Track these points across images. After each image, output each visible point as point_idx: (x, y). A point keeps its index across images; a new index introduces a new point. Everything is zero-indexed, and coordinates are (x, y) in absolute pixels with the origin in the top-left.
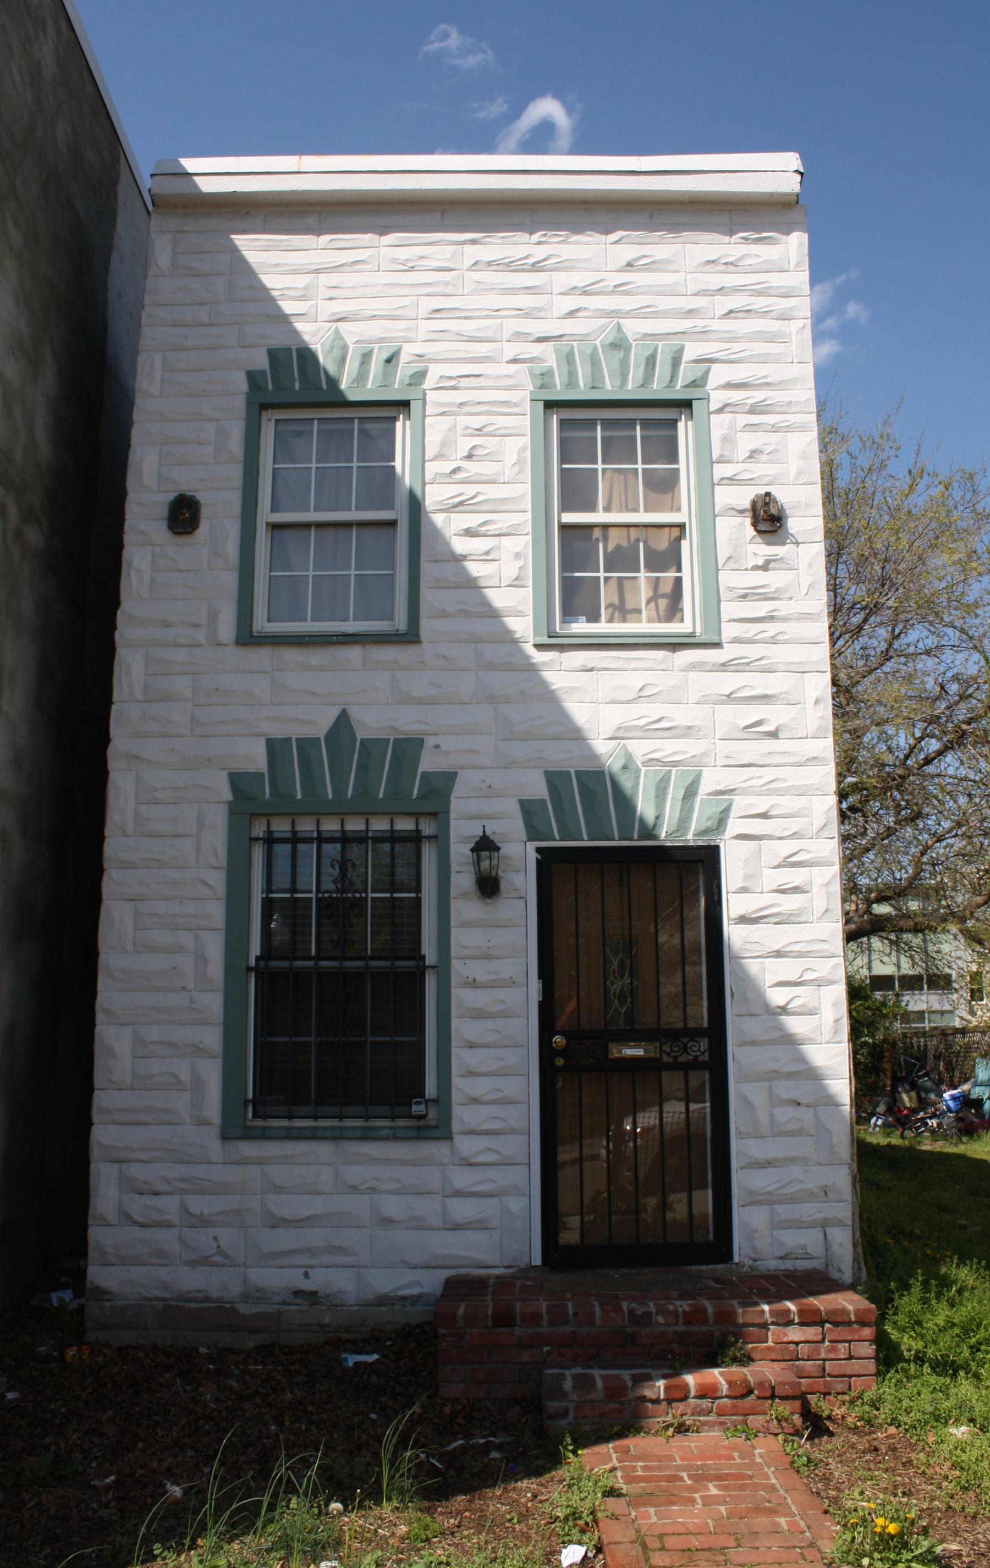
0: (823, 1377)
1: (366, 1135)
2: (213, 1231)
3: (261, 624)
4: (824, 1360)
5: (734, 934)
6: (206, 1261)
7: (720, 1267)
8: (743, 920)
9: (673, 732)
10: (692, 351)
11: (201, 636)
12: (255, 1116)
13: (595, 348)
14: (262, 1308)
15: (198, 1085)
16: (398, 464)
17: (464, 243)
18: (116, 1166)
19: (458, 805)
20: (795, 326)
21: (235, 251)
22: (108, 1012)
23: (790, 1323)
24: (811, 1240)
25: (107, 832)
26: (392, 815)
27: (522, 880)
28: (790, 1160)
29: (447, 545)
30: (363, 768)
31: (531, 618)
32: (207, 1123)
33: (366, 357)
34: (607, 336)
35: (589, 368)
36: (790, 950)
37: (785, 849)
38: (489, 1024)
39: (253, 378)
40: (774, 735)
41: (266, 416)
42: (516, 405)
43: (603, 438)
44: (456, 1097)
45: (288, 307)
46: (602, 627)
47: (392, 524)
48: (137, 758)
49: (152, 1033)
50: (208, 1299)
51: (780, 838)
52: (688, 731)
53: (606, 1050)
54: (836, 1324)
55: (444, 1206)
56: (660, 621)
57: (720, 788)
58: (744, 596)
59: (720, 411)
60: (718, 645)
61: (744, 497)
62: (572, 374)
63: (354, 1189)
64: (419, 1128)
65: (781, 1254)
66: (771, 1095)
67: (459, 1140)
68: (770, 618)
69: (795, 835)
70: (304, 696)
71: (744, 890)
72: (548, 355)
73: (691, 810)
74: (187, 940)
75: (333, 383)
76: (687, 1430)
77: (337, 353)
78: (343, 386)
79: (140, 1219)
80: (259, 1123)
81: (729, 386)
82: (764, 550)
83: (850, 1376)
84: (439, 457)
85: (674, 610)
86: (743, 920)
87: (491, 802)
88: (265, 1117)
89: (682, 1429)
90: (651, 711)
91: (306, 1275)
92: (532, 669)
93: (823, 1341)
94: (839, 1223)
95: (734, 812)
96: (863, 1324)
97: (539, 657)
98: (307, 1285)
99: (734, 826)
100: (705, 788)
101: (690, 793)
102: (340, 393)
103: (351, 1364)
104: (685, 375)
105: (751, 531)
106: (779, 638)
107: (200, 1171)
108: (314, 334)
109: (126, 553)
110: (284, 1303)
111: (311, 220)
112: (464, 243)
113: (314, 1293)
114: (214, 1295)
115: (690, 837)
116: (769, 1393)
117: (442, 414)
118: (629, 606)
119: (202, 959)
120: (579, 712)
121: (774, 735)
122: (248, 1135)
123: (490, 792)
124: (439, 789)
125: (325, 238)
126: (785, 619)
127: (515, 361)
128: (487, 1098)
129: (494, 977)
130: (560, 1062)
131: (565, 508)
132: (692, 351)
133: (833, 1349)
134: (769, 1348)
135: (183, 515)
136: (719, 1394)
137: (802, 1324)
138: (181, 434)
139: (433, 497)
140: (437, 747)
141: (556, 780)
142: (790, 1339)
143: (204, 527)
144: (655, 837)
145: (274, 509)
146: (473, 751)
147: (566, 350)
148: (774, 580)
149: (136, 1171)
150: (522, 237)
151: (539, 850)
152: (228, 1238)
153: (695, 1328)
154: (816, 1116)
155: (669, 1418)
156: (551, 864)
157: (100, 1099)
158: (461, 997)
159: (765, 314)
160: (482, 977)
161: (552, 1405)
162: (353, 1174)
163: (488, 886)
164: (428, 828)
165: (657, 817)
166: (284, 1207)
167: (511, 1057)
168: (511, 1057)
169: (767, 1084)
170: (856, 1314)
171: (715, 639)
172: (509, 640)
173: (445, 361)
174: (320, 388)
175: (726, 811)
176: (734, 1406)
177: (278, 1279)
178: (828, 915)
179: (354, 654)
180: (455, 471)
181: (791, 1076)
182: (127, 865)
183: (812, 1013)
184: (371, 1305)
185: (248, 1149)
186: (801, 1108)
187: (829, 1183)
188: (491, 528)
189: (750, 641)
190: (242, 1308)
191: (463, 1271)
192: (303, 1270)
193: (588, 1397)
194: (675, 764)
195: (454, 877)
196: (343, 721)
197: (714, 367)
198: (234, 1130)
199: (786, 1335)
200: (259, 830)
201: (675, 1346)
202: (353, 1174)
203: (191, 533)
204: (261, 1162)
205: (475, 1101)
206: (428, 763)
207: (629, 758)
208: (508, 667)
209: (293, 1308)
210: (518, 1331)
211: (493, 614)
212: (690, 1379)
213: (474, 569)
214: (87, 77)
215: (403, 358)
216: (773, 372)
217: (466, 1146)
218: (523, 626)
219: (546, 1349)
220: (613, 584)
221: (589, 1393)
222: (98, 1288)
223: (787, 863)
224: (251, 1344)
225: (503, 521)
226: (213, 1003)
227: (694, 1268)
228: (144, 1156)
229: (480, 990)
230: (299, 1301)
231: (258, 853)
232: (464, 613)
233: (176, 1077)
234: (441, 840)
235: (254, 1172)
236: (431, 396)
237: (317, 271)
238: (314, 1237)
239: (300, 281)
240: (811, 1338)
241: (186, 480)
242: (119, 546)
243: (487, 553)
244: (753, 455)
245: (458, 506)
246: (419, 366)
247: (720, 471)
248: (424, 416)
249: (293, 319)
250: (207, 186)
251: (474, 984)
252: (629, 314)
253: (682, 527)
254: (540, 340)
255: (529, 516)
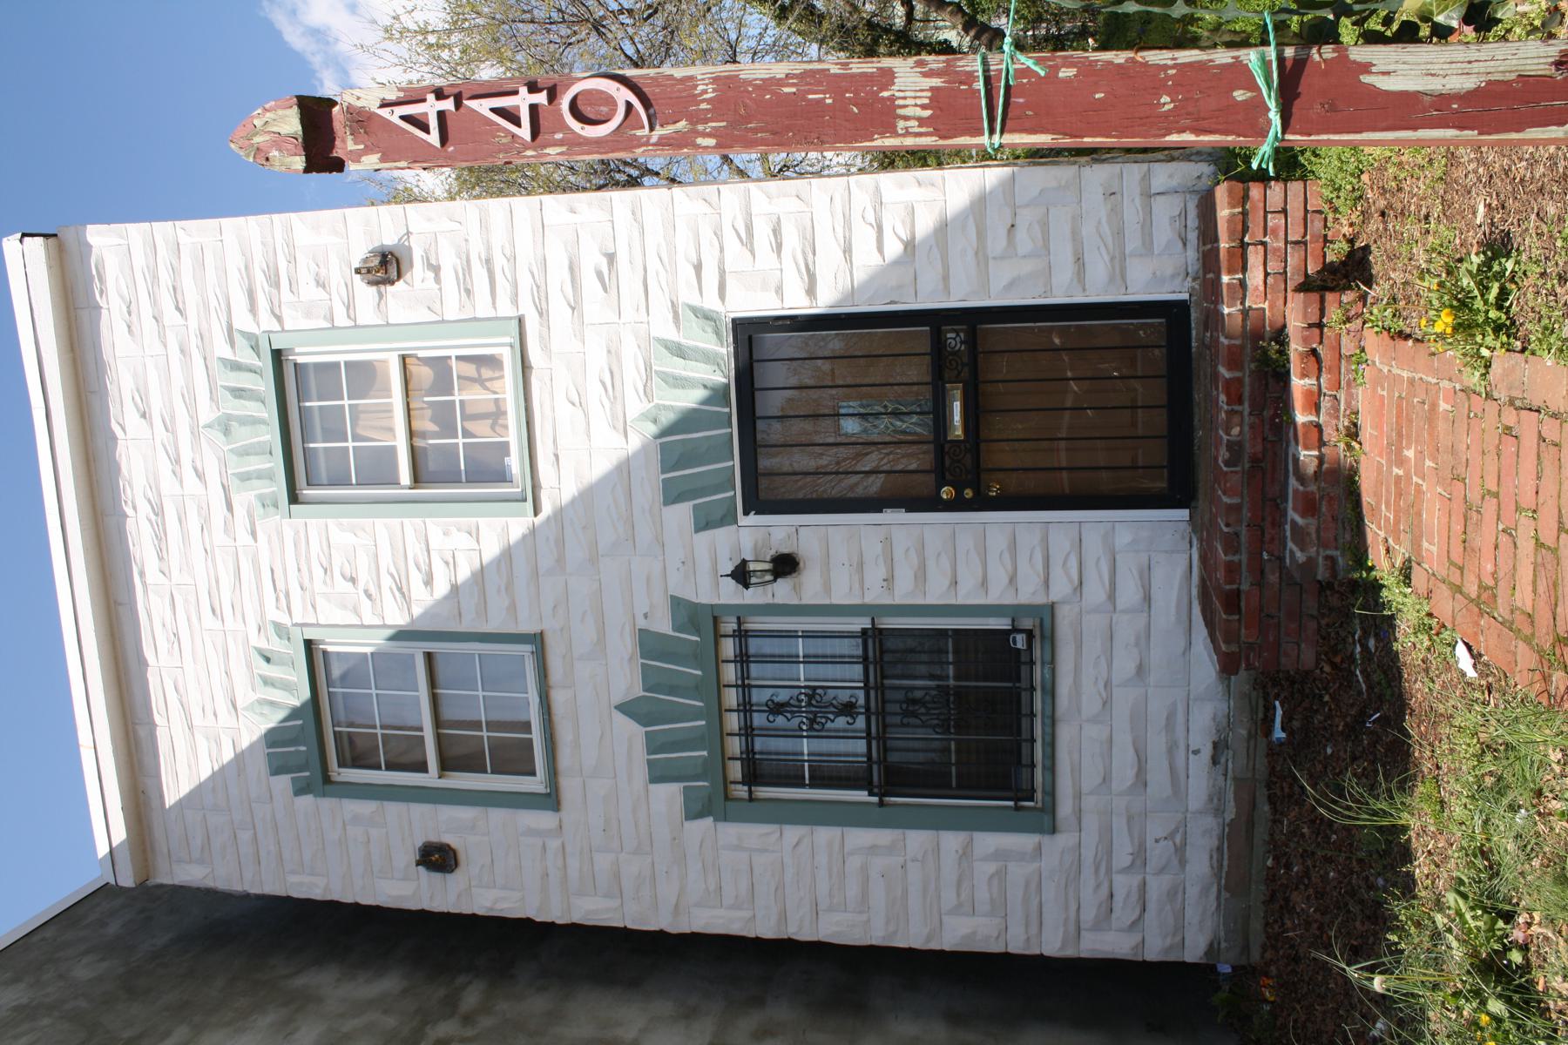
0: (1305, 243)
1: (1051, 692)
2: (1150, 843)
3: (535, 784)
4: (1286, 242)
5: (824, 302)
6: (1180, 850)
7: (1194, 315)
8: (811, 291)
9: (615, 370)
10: (222, 350)
11: (553, 844)
12: (1032, 799)
13: (231, 450)
14: (1230, 795)
15: (1000, 855)
16: (368, 650)
17: (144, 584)
18: (1083, 933)
19: (705, 597)
20: (184, 239)
21: (180, 803)
22: (928, 940)
23: (1243, 284)
24: (1166, 210)
25: (752, 935)
26: (718, 661)
27: (780, 531)
28: (1076, 237)
29: (439, 603)
30: (672, 690)
31: (509, 519)
32: (1039, 849)
33: (267, 682)
34: (218, 436)
35: (252, 458)
36: (845, 233)
37: (732, 245)
38: (931, 564)
39: (301, 789)
40: (611, 258)
41: (335, 777)
42: (297, 533)
43: (324, 441)
44: (1009, 600)
45: (228, 755)
46: (513, 436)
47: (429, 657)
48: (677, 906)
49: (949, 897)
50: (1220, 849)
51: (722, 250)
52: (613, 353)
53: (956, 442)
54: (1245, 229)
55: (1124, 611)
56: (502, 377)
57: (670, 316)
58: (468, 292)
59: (279, 319)
60: (521, 321)
61: (365, 293)
62: (260, 475)
63: (1107, 703)
64: (1043, 637)
65: (1180, 245)
66: (1002, 258)
67: (1053, 597)
68: (488, 262)
69: (718, 234)
70: (602, 745)
71: (779, 290)
72: (244, 498)
73: (696, 350)
74: (854, 863)
75: (295, 713)
76: (1355, 425)
77: (266, 710)
78: (297, 703)
79: (1137, 912)
80: (1039, 795)
81: (253, 309)
82: (418, 273)
83: (1306, 211)
84: (356, 611)
85: (492, 362)
86: (811, 291)
87: (698, 560)
88: (1033, 790)
89: (1353, 432)
90: (594, 392)
91: (1196, 752)
92: (559, 514)
93: (1264, 244)
94: (1146, 178)
95: (696, 302)
96: (1245, 197)
97: (547, 509)
98: (1207, 751)
99: (711, 302)
100: (671, 334)
101: (679, 351)
102: (304, 705)
103: (1283, 735)
104: (246, 356)
105: (400, 285)
106: (508, 254)
107: (1088, 855)
108: (252, 729)
109: (481, 912)
110: (1225, 775)
111: (142, 732)
112: (144, 584)
113: (1215, 745)
114: (1216, 843)
115: (724, 351)
116: (1316, 331)
117: (314, 607)
118: (492, 408)
119: (873, 849)
120: (601, 466)
121: (611, 258)
122: (1050, 808)
123: (689, 562)
124: (689, 614)
125: (157, 719)
126: (489, 248)
127: (254, 534)
128: (1009, 567)
129: (881, 560)
130: (968, 493)
131: (395, 483)
132: (222, 350)
133: (1275, 232)
134: (1271, 307)
135: (438, 858)
136: (1315, 388)
137: (1244, 269)
138: (359, 854)
139: (398, 618)
140: (646, 616)
141: (673, 494)
142: (1261, 283)
143: (448, 839)
144: (728, 386)
145: (422, 767)
146: (648, 580)
147: (237, 481)
148: (449, 262)
149: (1089, 915)
150: (130, 525)
151: (746, 513)
152: (1156, 828)
153: (1246, 394)
154: (1027, 206)
155: (1342, 445)
156: (757, 502)
157: (1016, 947)
158: (903, 593)
159: (174, 271)
160: (882, 572)
161: (1322, 573)
162: (1090, 703)
163: (785, 565)
164: (729, 626)
165: (705, 387)
166: (1124, 773)
167: (966, 541)
168: (966, 541)
169: (991, 263)
170: (1234, 207)
171: (515, 323)
172: (533, 531)
173: (262, 605)
174: (302, 726)
175: (695, 311)
176: (1330, 371)
177: (1200, 781)
178: (803, 196)
179: (558, 697)
180: (369, 596)
181: (981, 234)
182: (783, 917)
183: (912, 212)
184: (1229, 686)
185: (1065, 808)
186: (1018, 222)
187: (1101, 191)
188: (423, 559)
189: (515, 285)
190: (1230, 814)
191: (1195, 592)
192: (1191, 756)
193: (1314, 536)
194: (648, 367)
195: (779, 600)
196: (626, 708)
197: (236, 325)
198: (1046, 821)
199: (1257, 288)
200: (741, 791)
201: (1267, 414)
202: (1090, 703)
203: (454, 852)
204: (1078, 796)
205: (1013, 579)
206: (663, 624)
207: (644, 416)
208: (561, 542)
209: (1230, 765)
210: (1245, 587)
211: (507, 555)
212: (1301, 418)
213: (464, 573)
214: (35, 938)
215: (263, 645)
216: (234, 262)
217: (1060, 589)
218: (517, 525)
219: (1265, 556)
220: (470, 426)
221: (1309, 534)
222: (1206, 954)
223: (748, 240)
224: (1267, 808)
225: (415, 549)
226: (917, 840)
227: (1194, 344)
228: (1073, 908)
229: (896, 573)
230: (1223, 760)
231: (764, 792)
232: (509, 586)
233: (992, 877)
234: (741, 613)
235: (1089, 802)
236: (298, 619)
237: (191, 727)
238: (1157, 745)
239: (202, 745)
240: (1261, 259)
241: (406, 856)
242: (474, 918)
243: (447, 563)
244: (321, 284)
245: (402, 591)
246: (271, 630)
247: (341, 320)
248: (318, 625)
249: (238, 750)
250: (120, 834)
251: (889, 580)
252: (194, 417)
253: (404, 358)
254: (230, 507)
255: (406, 521)
